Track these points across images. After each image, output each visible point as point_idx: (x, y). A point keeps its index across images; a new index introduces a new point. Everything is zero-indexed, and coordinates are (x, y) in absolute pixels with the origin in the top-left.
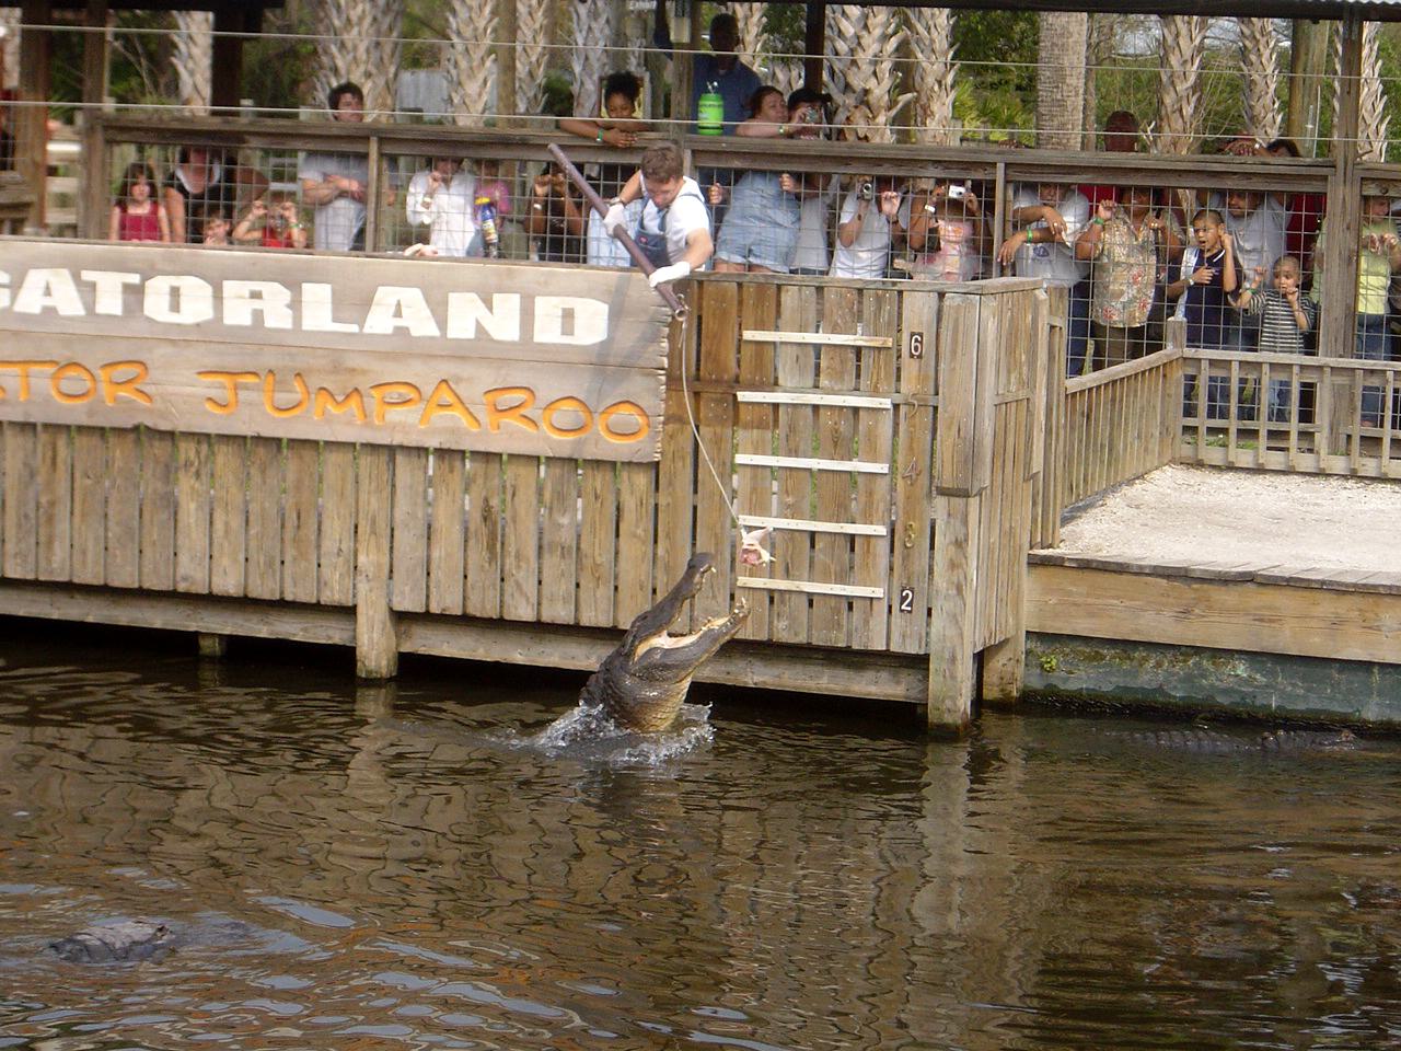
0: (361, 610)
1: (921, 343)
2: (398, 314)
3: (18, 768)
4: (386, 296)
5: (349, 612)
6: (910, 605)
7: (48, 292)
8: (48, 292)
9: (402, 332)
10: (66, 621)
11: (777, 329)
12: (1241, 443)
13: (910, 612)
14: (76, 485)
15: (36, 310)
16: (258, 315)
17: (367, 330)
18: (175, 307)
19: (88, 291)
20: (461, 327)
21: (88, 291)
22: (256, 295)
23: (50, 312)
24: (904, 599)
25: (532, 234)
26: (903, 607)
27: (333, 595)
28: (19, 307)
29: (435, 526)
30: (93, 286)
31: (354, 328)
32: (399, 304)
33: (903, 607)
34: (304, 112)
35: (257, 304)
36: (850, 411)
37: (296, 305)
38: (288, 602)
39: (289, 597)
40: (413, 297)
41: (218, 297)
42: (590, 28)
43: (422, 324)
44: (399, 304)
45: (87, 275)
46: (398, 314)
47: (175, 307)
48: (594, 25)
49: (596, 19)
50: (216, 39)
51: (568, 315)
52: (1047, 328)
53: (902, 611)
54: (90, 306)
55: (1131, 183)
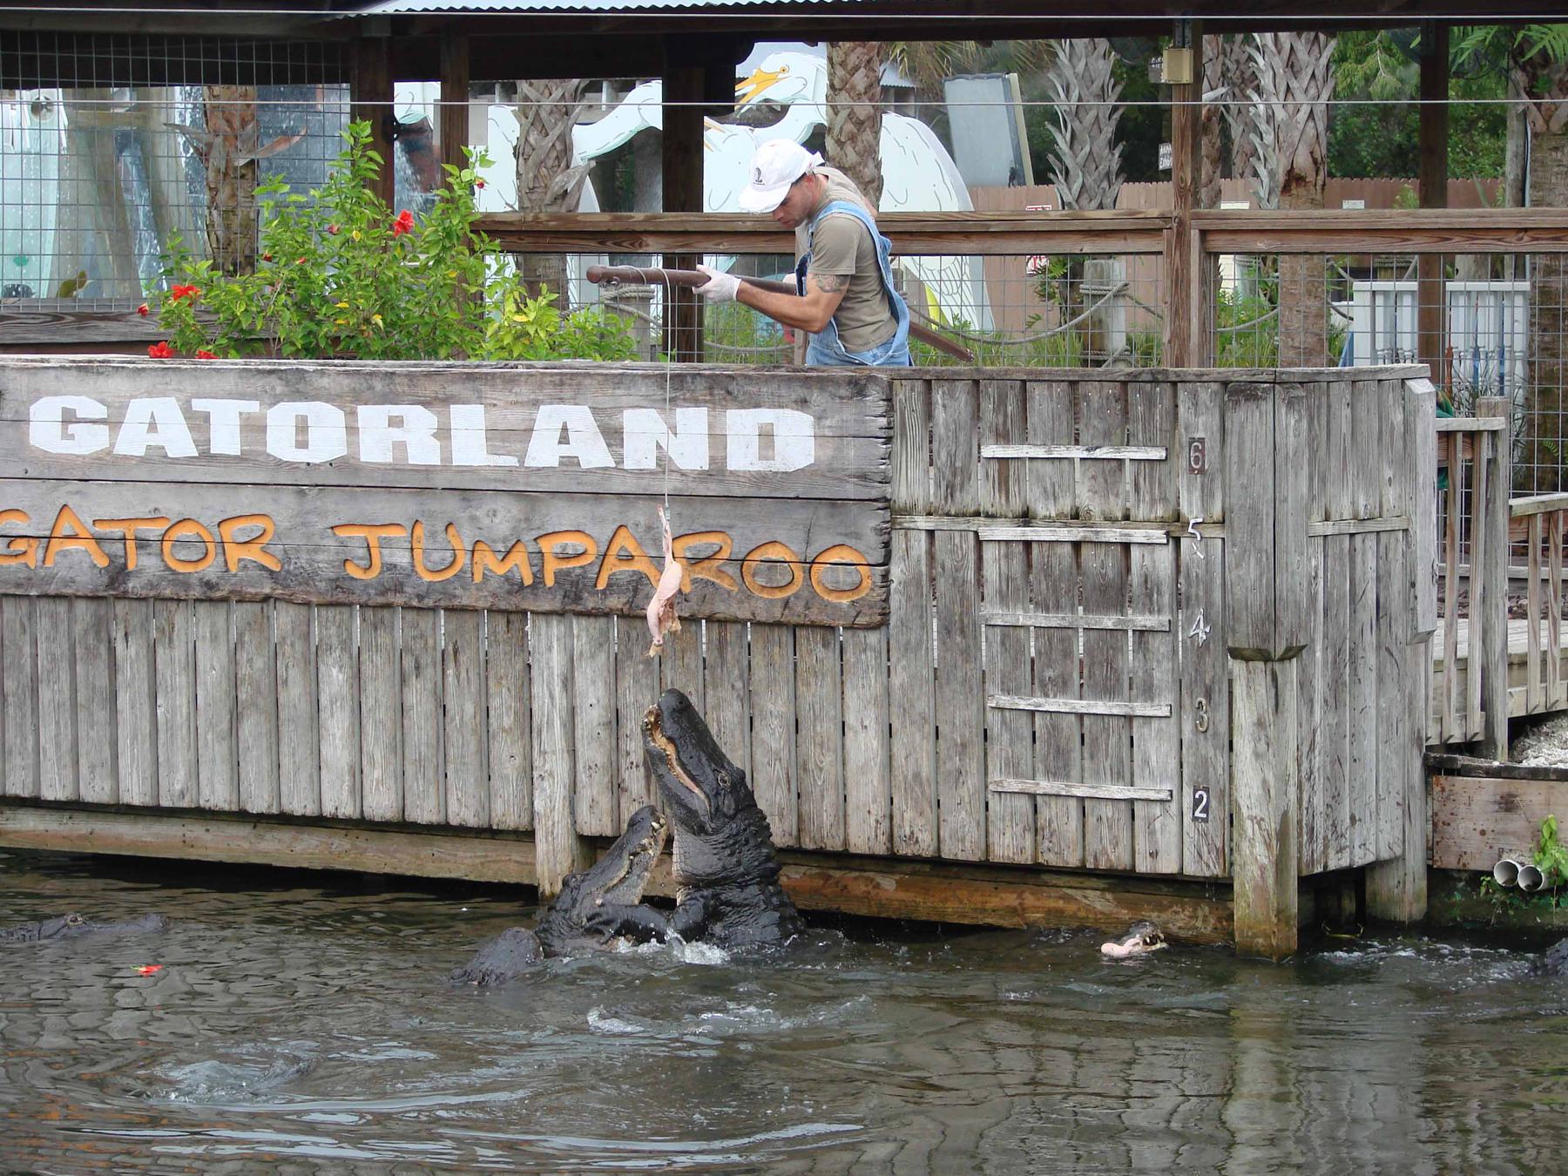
0: (539, 835)
1: (1202, 451)
2: (564, 439)
3: (1398, 804)
4: (139, 409)
5: (526, 836)
8: (153, 427)
9: (570, 462)
11: (1024, 440)
16: (400, 447)
17: (530, 462)
18: (302, 444)
19: (199, 424)
20: (639, 455)
21: (199, 424)
22: (395, 422)
23: (570, 462)
24: (1197, 802)
26: (1197, 814)
27: (506, 814)
28: (120, 449)
29: (623, 712)
30: (206, 417)
31: (511, 461)
32: (565, 429)
33: (1197, 814)
34: (638, 216)
35: (397, 434)
36: (1021, 546)
37: (443, 433)
39: (454, 821)
43: (593, 453)
44: (565, 429)
46: (564, 439)
47: (302, 444)
50: (241, 83)
51: (302, 427)
52: (1433, 440)
53: (1195, 819)
54: (203, 443)
55: (198, 31)
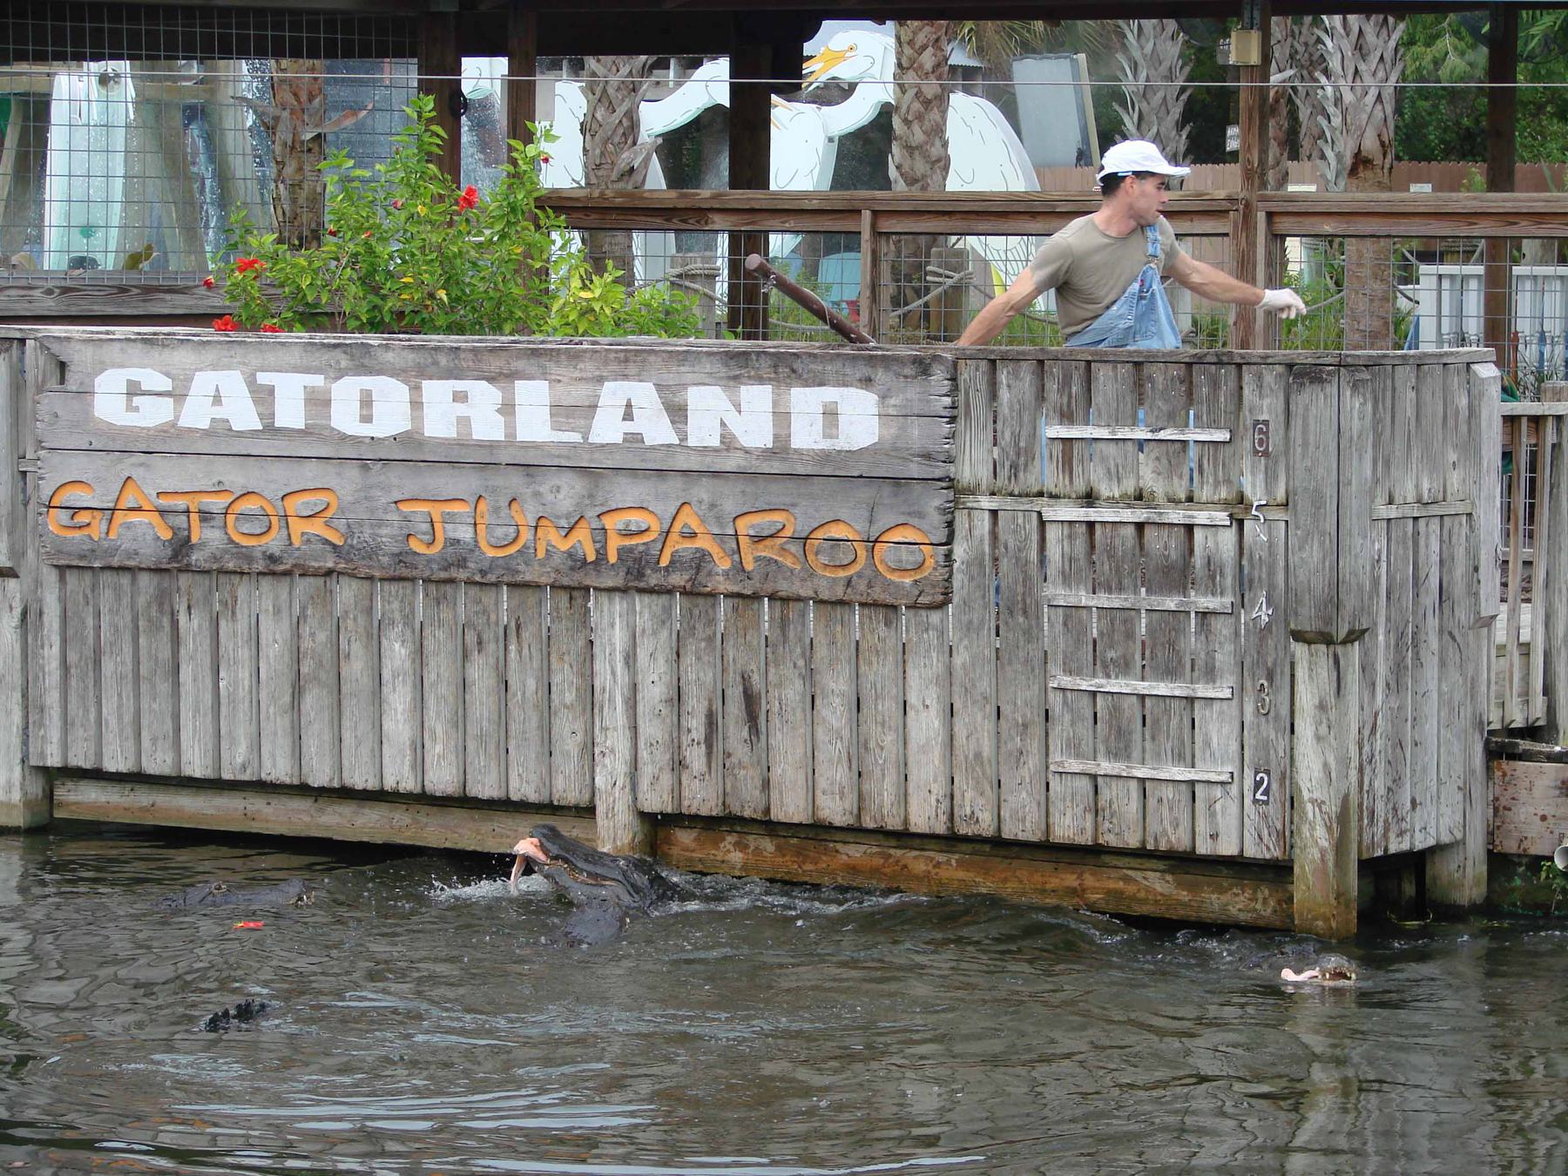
2: (628, 416)
6: (1266, 793)
7: (217, 400)
8: (217, 400)
9: (634, 439)
10: (251, 833)
12: (833, 406)
13: (1266, 803)
14: (221, 632)
15: (204, 424)
16: (464, 422)
18: (367, 419)
19: (264, 397)
20: (703, 432)
21: (264, 397)
22: (460, 397)
24: (1258, 785)
25: (923, 333)
26: (1258, 796)
28: (184, 422)
30: (271, 391)
31: (575, 437)
32: (629, 406)
33: (1258, 796)
35: (461, 409)
37: (508, 409)
38: (515, 803)
39: (515, 797)
40: (644, 394)
41: (416, 405)
42: (1356, 71)
43: (657, 430)
44: (629, 406)
45: (263, 378)
46: (628, 416)
47: (367, 419)
48: (1362, 67)
49: (1364, 57)
